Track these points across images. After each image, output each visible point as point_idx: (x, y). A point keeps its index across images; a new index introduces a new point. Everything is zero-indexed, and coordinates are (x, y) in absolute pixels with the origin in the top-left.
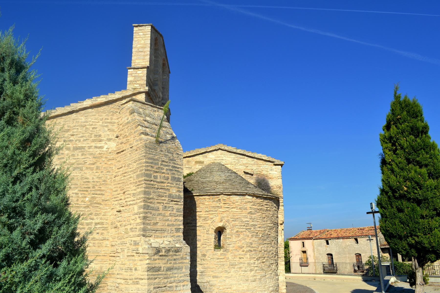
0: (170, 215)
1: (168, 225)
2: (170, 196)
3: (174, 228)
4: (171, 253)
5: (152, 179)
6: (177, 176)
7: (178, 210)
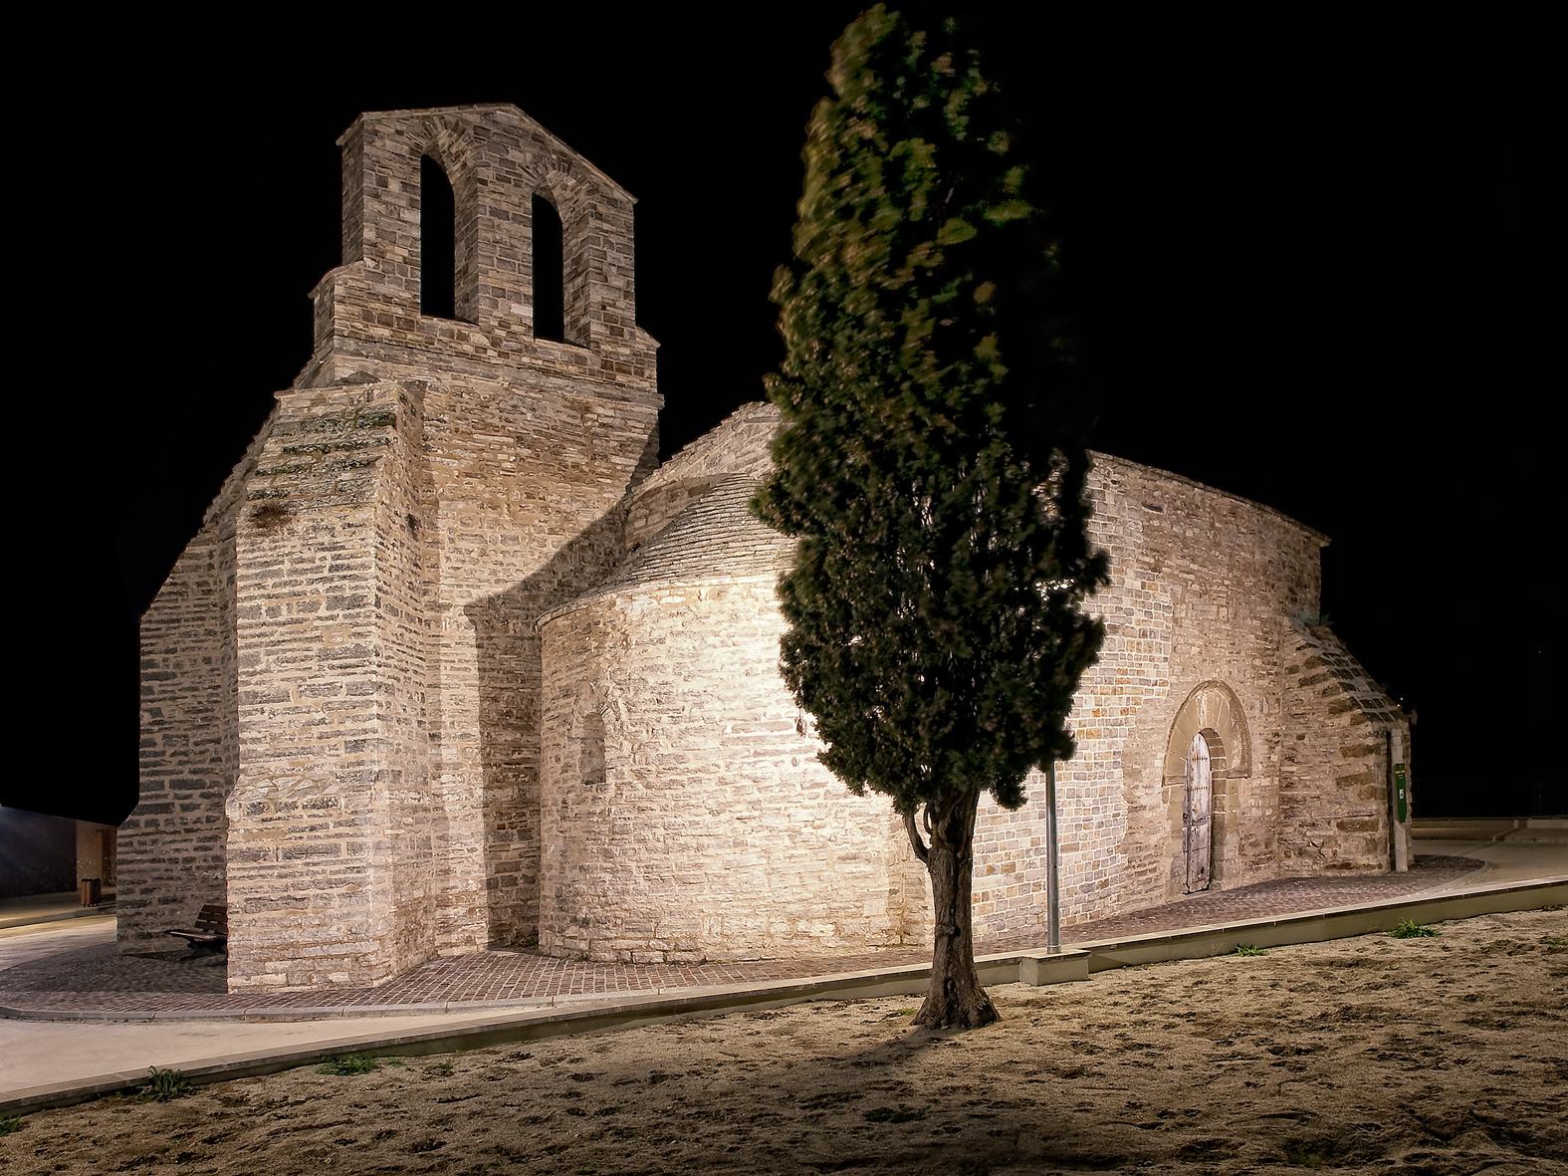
5: (265, 618)
6: (348, 593)
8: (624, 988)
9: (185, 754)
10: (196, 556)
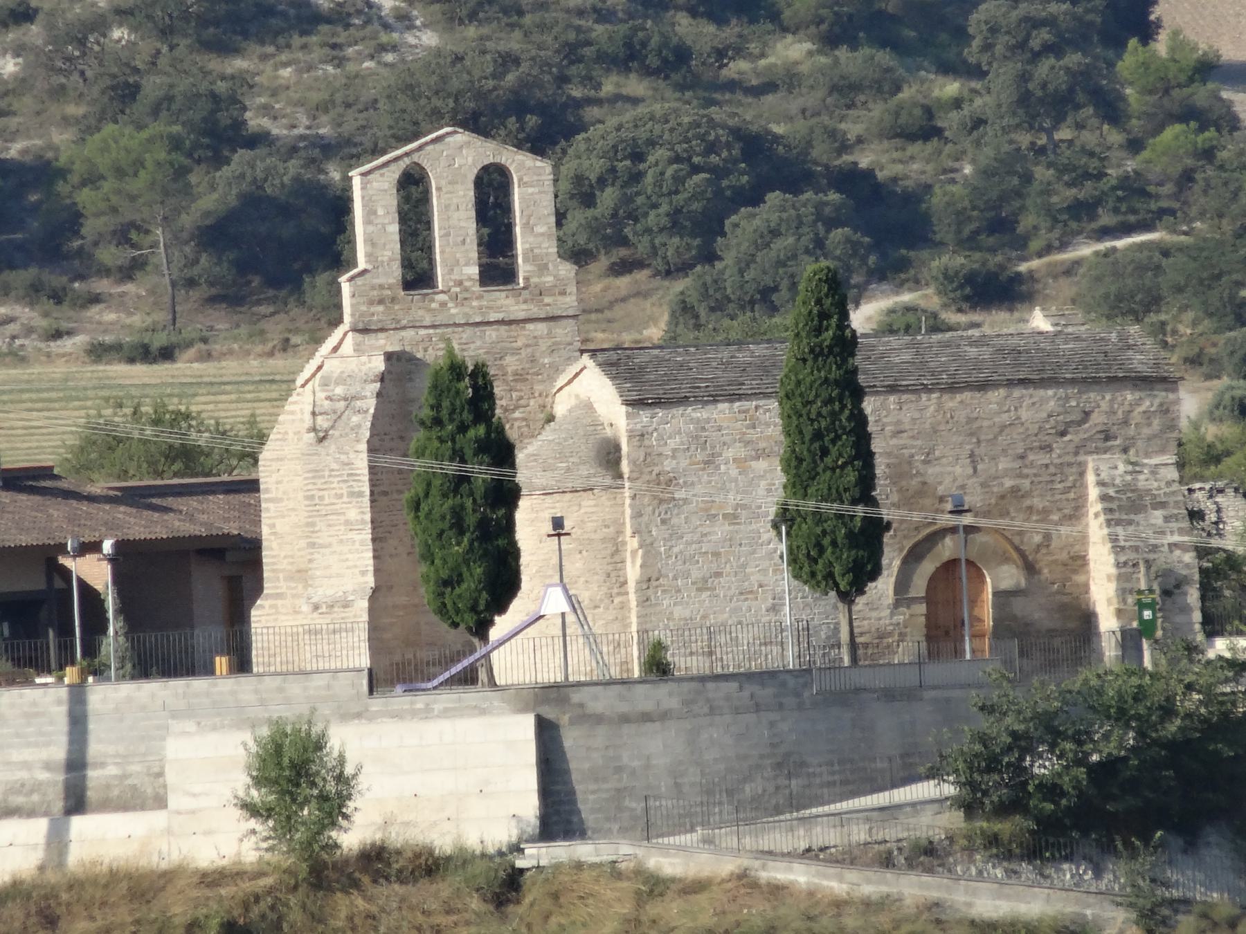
0: (350, 552)
1: (348, 568)
2: (347, 522)
3: (357, 571)
4: (336, 609)
5: (317, 501)
6: (357, 489)
7: (362, 543)
8: (627, 593)
9: (292, 557)
10: (292, 413)
